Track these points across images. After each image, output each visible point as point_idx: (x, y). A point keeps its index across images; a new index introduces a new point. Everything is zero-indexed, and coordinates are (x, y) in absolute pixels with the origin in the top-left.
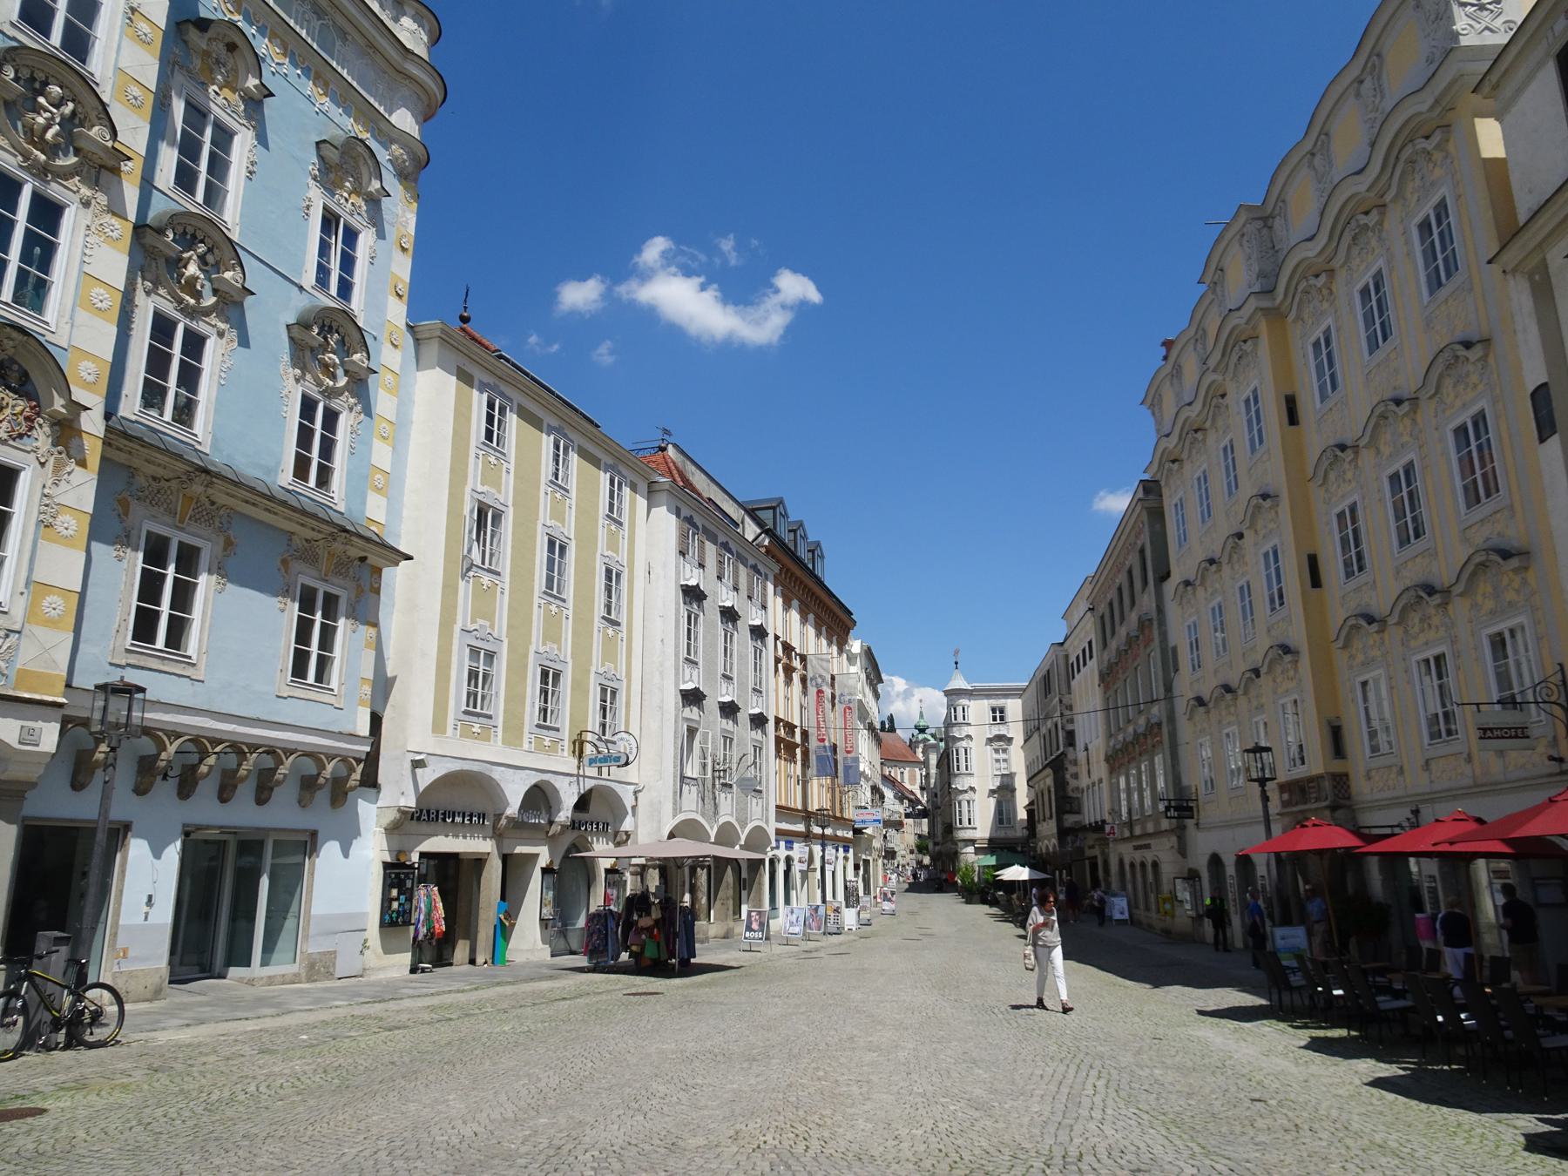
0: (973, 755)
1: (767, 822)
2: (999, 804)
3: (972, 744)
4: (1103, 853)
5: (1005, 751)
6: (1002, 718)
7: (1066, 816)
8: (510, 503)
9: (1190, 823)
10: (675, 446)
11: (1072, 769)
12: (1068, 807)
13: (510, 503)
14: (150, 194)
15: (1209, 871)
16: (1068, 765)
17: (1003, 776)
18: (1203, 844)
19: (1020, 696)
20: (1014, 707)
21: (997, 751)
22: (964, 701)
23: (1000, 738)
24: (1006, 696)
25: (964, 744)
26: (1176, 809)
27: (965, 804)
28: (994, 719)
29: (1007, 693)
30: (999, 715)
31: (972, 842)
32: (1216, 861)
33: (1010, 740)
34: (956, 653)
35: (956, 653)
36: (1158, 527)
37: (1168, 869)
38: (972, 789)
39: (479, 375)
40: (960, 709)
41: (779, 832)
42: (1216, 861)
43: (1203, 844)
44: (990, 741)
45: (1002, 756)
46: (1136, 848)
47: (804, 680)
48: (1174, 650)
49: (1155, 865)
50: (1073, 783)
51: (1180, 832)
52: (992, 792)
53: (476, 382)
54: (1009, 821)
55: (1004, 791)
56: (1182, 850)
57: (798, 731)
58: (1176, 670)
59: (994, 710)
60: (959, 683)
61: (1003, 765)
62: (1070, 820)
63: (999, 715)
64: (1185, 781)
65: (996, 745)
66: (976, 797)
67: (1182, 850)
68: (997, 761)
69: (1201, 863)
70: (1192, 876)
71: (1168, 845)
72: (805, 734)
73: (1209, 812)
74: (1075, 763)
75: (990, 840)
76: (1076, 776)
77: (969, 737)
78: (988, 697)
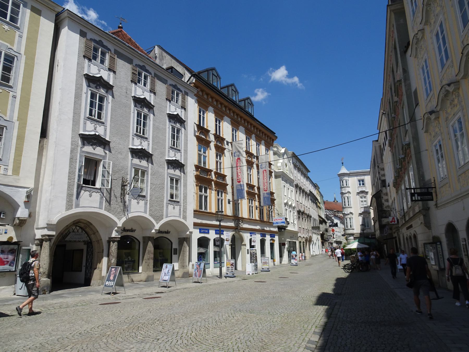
0: (352, 200)
1: (185, 218)
2: (364, 219)
3: (350, 195)
4: (398, 234)
5: (365, 197)
6: (363, 184)
7: (383, 219)
8: (22, 52)
9: (431, 204)
10: (159, 46)
11: (385, 197)
12: (384, 215)
13: (22, 52)
14: (298, 158)
15: (447, 236)
16: (382, 195)
17: (365, 207)
18: (441, 218)
19: (369, 174)
20: (368, 179)
21: (361, 197)
22: (346, 178)
23: (362, 192)
24: (364, 175)
25: (347, 195)
26: (419, 194)
27: (348, 220)
28: (360, 184)
29: (364, 174)
30: (362, 182)
31: (353, 235)
32: (451, 229)
33: (367, 193)
34: (342, 159)
35: (342, 159)
36: (402, 21)
37: (421, 239)
38: (351, 213)
39: (44, 10)
40: (344, 182)
41: (196, 225)
42: (451, 229)
43: (441, 218)
44: (358, 193)
45: (364, 199)
46: (408, 228)
47: (258, 166)
48: (416, 92)
49: (415, 236)
50: (386, 204)
51: (425, 211)
52: (360, 214)
53: (29, 6)
54: (368, 226)
55: (365, 214)
56: (428, 224)
57: (256, 188)
58: (417, 104)
59: (359, 181)
60: (344, 170)
61: (365, 203)
62: (385, 221)
63: (362, 182)
64: (427, 178)
65: (361, 195)
66: (353, 216)
67: (428, 224)
68: (362, 201)
69: (440, 231)
70: (436, 241)
71: (420, 222)
72: (259, 188)
73: (444, 194)
74: (387, 194)
75: (360, 234)
76: (387, 201)
77: (349, 192)
78: (357, 176)
